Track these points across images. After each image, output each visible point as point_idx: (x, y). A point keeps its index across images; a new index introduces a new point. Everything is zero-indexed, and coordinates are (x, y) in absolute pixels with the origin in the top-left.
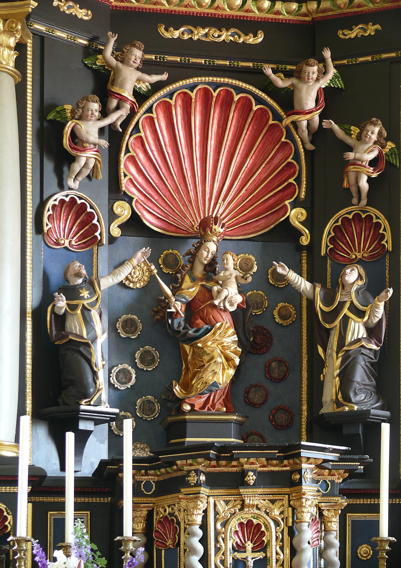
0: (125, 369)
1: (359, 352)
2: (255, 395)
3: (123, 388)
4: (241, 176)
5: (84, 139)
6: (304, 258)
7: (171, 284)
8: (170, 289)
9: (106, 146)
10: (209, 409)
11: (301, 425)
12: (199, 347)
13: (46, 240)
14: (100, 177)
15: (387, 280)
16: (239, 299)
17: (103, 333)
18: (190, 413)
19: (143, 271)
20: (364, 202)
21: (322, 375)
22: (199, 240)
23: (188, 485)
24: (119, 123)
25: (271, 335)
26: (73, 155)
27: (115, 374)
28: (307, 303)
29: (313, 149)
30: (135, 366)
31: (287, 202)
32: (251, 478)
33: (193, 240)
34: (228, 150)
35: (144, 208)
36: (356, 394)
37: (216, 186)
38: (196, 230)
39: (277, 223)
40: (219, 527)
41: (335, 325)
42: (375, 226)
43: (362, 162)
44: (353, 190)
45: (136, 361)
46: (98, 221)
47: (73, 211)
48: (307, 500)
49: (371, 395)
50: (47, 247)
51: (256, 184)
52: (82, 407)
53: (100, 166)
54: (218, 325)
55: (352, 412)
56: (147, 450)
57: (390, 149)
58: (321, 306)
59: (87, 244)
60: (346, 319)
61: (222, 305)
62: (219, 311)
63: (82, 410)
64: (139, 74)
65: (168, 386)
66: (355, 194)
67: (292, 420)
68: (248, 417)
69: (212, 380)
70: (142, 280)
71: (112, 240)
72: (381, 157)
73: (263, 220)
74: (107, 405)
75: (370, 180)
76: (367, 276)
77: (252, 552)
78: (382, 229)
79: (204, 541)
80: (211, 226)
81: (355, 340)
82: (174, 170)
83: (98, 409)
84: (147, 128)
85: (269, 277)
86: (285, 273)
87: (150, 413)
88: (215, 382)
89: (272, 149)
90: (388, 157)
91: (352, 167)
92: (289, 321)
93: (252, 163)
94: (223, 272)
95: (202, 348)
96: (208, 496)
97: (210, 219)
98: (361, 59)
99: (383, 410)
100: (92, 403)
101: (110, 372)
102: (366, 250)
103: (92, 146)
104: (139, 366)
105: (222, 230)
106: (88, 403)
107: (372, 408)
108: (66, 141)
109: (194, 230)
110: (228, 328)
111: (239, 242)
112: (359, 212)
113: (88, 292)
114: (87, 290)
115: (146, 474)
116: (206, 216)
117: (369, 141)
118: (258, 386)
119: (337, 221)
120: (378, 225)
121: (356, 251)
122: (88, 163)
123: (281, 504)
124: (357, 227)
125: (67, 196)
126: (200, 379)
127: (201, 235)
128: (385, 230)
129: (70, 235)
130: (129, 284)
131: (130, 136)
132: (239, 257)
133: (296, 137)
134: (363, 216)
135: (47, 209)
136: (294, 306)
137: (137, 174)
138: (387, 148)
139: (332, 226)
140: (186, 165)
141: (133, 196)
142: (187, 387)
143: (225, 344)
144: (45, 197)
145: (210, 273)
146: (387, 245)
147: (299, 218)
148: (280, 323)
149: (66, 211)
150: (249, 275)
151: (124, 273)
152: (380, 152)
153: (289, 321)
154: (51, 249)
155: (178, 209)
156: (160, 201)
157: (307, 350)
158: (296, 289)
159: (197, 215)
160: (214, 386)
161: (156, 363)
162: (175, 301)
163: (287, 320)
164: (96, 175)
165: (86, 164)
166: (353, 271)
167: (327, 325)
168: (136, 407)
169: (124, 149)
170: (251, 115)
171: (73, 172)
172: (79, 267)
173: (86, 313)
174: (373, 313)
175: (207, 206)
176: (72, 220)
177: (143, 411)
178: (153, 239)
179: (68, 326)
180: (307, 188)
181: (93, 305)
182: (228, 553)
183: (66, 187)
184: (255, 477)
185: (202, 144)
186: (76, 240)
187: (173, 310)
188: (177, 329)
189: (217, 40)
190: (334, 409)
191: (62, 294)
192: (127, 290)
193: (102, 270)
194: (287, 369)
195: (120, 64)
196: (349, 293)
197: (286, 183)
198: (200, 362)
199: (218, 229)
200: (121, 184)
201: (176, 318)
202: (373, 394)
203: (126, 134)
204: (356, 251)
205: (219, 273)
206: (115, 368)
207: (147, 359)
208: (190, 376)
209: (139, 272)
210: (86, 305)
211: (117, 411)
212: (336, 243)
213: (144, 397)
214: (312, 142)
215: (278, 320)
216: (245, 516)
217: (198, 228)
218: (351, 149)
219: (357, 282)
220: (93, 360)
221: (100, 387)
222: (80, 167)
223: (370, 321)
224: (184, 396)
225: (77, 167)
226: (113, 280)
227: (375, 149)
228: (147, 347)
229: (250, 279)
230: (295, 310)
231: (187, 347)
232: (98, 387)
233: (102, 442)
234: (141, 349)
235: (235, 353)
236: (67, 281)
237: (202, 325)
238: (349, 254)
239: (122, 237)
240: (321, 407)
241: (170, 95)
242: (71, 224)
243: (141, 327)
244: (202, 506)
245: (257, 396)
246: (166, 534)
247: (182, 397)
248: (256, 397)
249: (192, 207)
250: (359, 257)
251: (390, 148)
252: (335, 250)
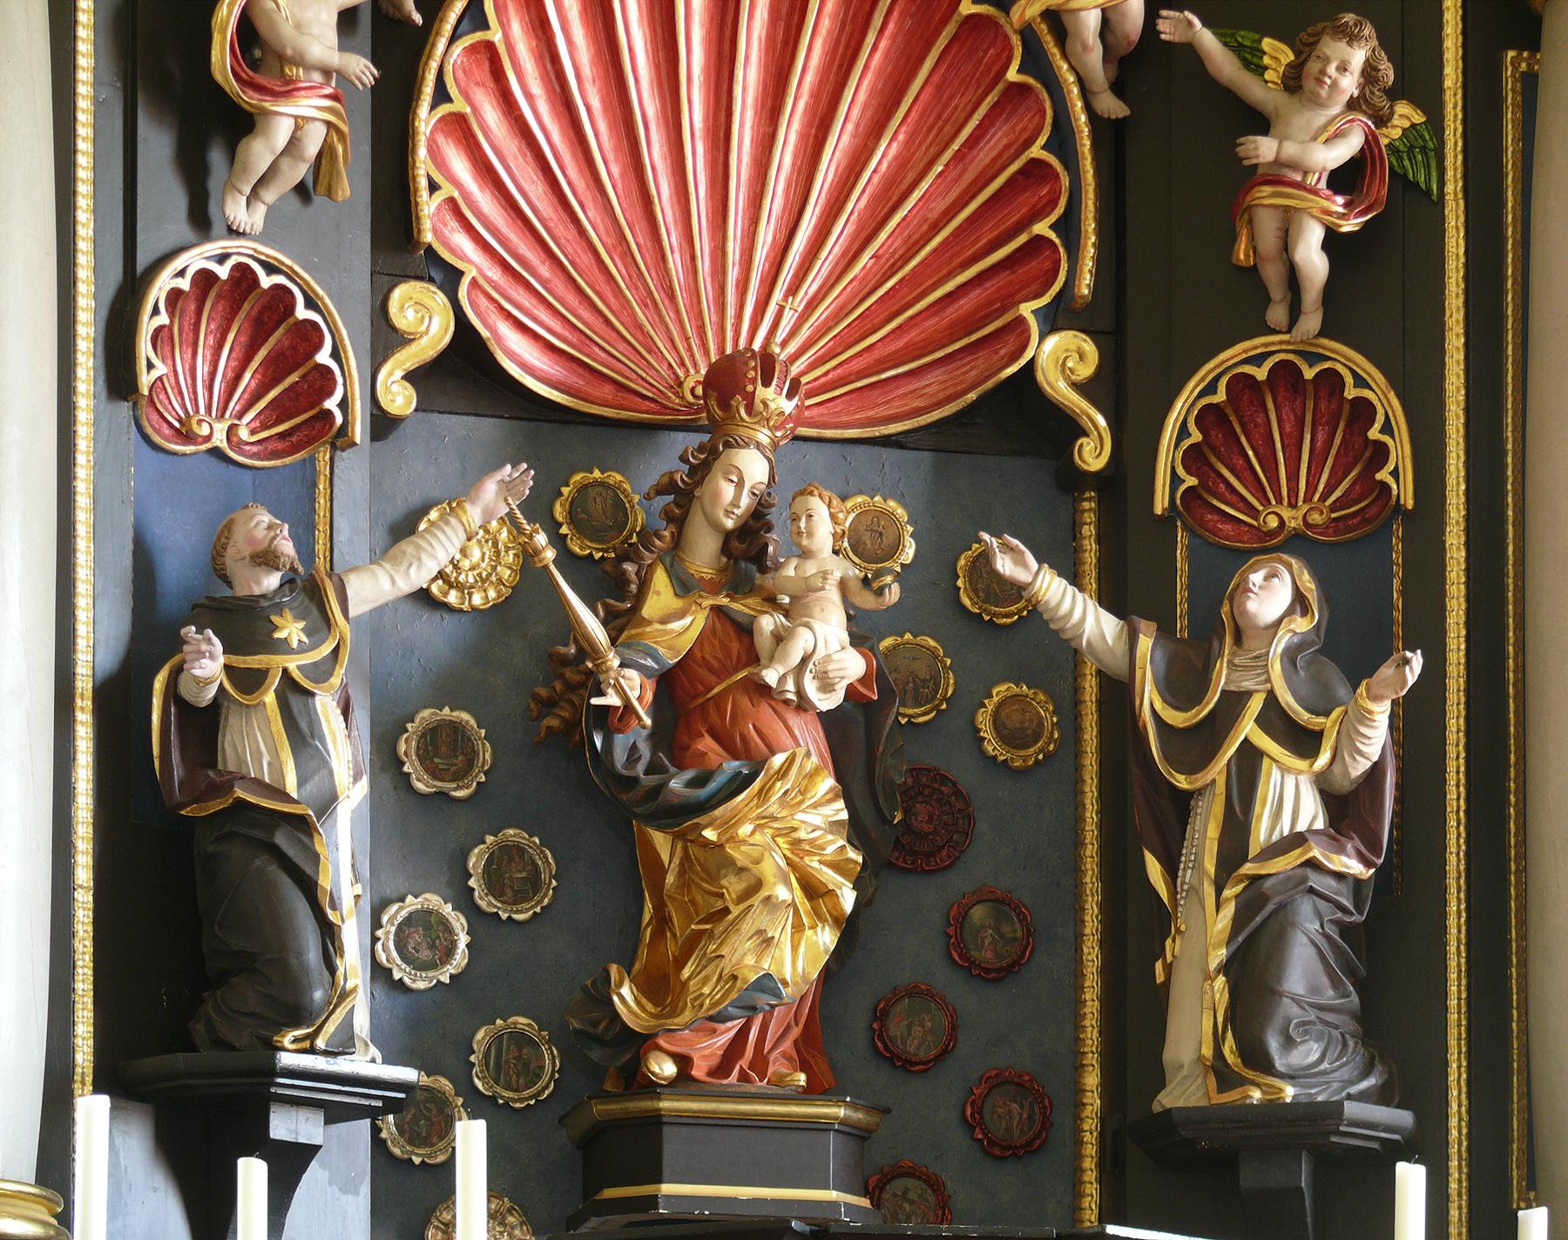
0: (429, 912)
1: (1297, 883)
2: (910, 1026)
3: (421, 985)
4: (857, 202)
5: (289, 52)
6: (1089, 517)
7: (600, 598)
8: (597, 615)
9: (369, 80)
10: (744, 1077)
11: (1080, 1143)
12: (706, 843)
13: (145, 423)
14: (344, 190)
15: (1398, 616)
16: (853, 666)
17: (357, 778)
18: (677, 1091)
19: (495, 544)
20: (1311, 322)
21: (1159, 965)
22: (706, 438)
25: (968, 804)
26: (246, 107)
27: (393, 929)
28: (1101, 686)
29: (1121, 116)
30: (465, 902)
31: (1027, 309)
33: (681, 435)
34: (807, 103)
35: (501, 309)
36: (1289, 1043)
37: (766, 236)
38: (690, 398)
39: (989, 384)
41: (1209, 778)
42: (1351, 414)
43: (1306, 173)
44: (1273, 275)
45: (472, 883)
46: (335, 355)
47: (242, 315)
49: (1345, 1045)
50: (145, 448)
51: (910, 237)
52: (287, 1059)
53: (345, 150)
54: (778, 760)
55: (1273, 1107)
56: (511, 1219)
57: (1404, 130)
58: (1159, 705)
59: (294, 439)
60: (1250, 760)
61: (790, 686)
62: (781, 708)
63: (283, 1069)
65: (593, 983)
66: (1277, 291)
67: (1046, 1124)
68: (887, 1111)
69: (756, 968)
70: (494, 578)
71: (383, 424)
72: (1373, 158)
73: (938, 372)
74: (374, 1051)
75: (1333, 242)
76: (1327, 600)
78: (1377, 426)
80: (750, 388)
81: (1283, 838)
82: (610, 170)
83: (342, 1065)
84: (512, 11)
85: (960, 583)
86: (1022, 576)
87: (521, 1081)
88: (768, 976)
89: (969, 107)
90: (1400, 159)
91: (1267, 190)
92: (1033, 753)
93: (896, 158)
94: (794, 562)
95: (719, 846)
97: (746, 364)
99: (1388, 1105)
100: (320, 1043)
101: (376, 924)
102: (1316, 498)
103: (317, 77)
104: (480, 902)
105: (788, 406)
106: (307, 1044)
107: (1349, 1097)
108: (221, 57)
109: (683, 398)
110: (812, 776)
111: (848, 448)
112: (1291, 357)
113: (302, 625)
114: (297, 618)
116: (729, 351)
117: (1330, 97)
118: (918, 993)
119: (1211, 389)
120: (1363, 412)
121: (1279, 501)
122: (299, 140)
124: (1286, 411)
125: (222, 259)
126: (712, 960)
127: (710, 417)
128: (1387, 428)
129: (232, 405)
130: (446, 594)
131: (453, 39)
132: (849, 504)
133: (1060, 68)
134: (1309, 373)
135: (149, 308)
136: (1052, 696)
137: (476, 180)
138: (1394, 127)
139: (1193, 404)
140: (655, 152)
143: (802, 834)
144: (143, 260)
145: (743, 565)
146: (1394, 486)
147: (1071, 370)
148: (1002, 758)
149: (218, 316)
150: (889, 579)
151: (434, 557)
152: (1371, 142)
153: (1033, 753)
154: (162, 456)
155: (626, 318)
156: (560, 286)
157: (1101, 865)
158: (1065, 636)
159: (694, 343)
160: (763, 991)
161: (546, 895)
162: (622, 665)
163: (1026, 746)
164: (330, 185)
165: (294, 144)
166: (1276, 580)
167: (1181, 778)
168: (473, 1058)
171: (245, 170)
172: (270, 527)
173: (295, 701)
174: (1348, 741)
175: (730, 311)
176: (237, 348)
177: (497, 1072)
178: (532, 425)
179: (229, 750)
180: (1099, 260)
181: (321, 672)
183: (218, 227)
185: (713, 79)
186: (253, 425)
187: (612, 699)
188: (624, 772)
190: (1207, 1093)
191: (210, 632)
192: (436, 616)
193: (350, 541)
194: (1029, 931)
196: (1263, 659)
197: (1022, 239)
198: (712, 900)
199: (776, 400)
200: (418, 218)
201: (620, 731)
202: (1351, 1043)
203: (438, 33)
204: (1279, 501)
205: (778, 567)
206: (395, 907)
207: (510, 878)
208: (672, 949)
209: (482, 547)
210: (297, 675)
211: (408, 1074)
212: (1206, 469)
213: (499, 1022)
214: (1118, 88)
215: (992, 747)
217: (699, 391)
218: (1261, 123)
219: (1290, 622)
220: (325, 882)
221: (349, 985)
222: (272, 152)
223: (1337, 769)
224: (653, 1022)
225: (260, 152)
226: (393, 582)
227: (1350, 129)
228: (511, 832)
229: (894, 594)
230: (1054, 713)
231: (661, 842)
232: (342, 983)
233: (349, 1188)
234: (490, 839)
235: (837, 866)
237: (721, 760)
238: (1254, 513)
239: (420, 415)
240: (1160, 1083)
242: (233, 364)
243: (488, 756)
245: (917, 1029)
247: (645, 1028)
249: (678, 312)
250: (1293, 524)
251: (1407, 124)
252: (1206, 496)
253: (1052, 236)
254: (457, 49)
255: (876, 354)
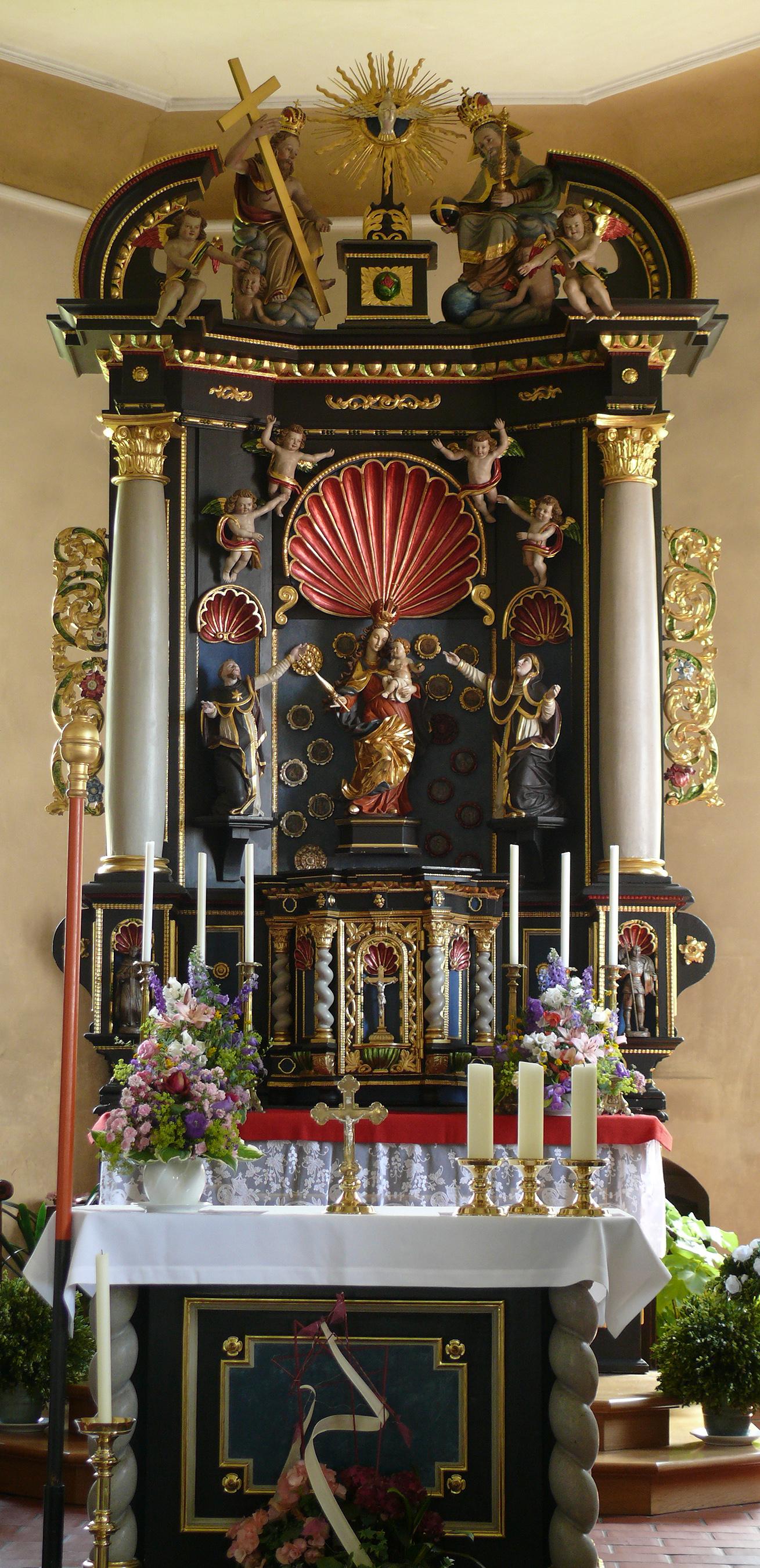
3: (293, 786)
10: (378, 811)
16: (412, 689)
23: (316, 907)
24: (280, 508)
30: (306, 761)
31: (468, 579)
32: (380, 901)
40: (349, 950)
46: (259, 612)
48: (437, 923)
54: (387, 719)
55: (519, 818)
58: (494, 699)
60: (517, 717)
61: (393, 697)
64: (302, 455)
75: (546, 561)
77: (385, 976)
79: (334, 965)
83: (249, 817)
86: (455, 664)
96: (338, 919)
98: (541, 425)
100: (242, 812)
103: (247, 540)
115: (287, 892)
120: (560, 607)
123: (413, 926)
134: (545, 597)
141: (300, 580)
142: (357, 785)
152: (557, 530)
153: (476, 708)
165: (242, 557)
169: (288, 531)
170: (426, 487)
175: (385, 583)
177: (316, 810)
181: (245, 707)
182: (359, 977)
184: (383, 900)
189: (388, 408)
195: (279, 449)
202: (546, 797)
210: (238, 708)
216: (379, 938)
225: (232, 563)
236: (222, 681)
238: (534, 636)
241: (337, 472)
244: (330, 928)
246: (305, 955)
248: (440, 792)
253: (475, 557)
254: (297, 521)
255: (427, 594)
